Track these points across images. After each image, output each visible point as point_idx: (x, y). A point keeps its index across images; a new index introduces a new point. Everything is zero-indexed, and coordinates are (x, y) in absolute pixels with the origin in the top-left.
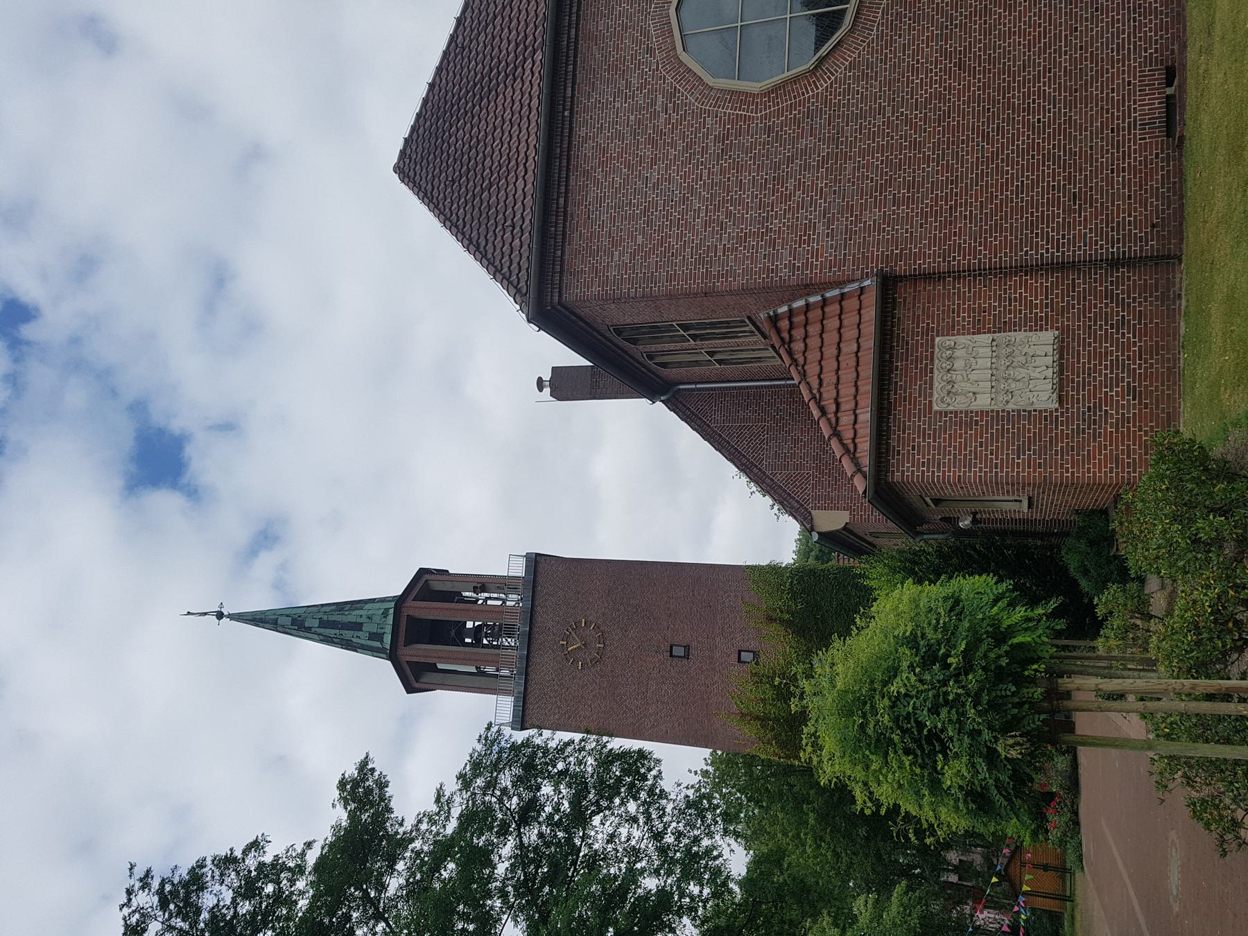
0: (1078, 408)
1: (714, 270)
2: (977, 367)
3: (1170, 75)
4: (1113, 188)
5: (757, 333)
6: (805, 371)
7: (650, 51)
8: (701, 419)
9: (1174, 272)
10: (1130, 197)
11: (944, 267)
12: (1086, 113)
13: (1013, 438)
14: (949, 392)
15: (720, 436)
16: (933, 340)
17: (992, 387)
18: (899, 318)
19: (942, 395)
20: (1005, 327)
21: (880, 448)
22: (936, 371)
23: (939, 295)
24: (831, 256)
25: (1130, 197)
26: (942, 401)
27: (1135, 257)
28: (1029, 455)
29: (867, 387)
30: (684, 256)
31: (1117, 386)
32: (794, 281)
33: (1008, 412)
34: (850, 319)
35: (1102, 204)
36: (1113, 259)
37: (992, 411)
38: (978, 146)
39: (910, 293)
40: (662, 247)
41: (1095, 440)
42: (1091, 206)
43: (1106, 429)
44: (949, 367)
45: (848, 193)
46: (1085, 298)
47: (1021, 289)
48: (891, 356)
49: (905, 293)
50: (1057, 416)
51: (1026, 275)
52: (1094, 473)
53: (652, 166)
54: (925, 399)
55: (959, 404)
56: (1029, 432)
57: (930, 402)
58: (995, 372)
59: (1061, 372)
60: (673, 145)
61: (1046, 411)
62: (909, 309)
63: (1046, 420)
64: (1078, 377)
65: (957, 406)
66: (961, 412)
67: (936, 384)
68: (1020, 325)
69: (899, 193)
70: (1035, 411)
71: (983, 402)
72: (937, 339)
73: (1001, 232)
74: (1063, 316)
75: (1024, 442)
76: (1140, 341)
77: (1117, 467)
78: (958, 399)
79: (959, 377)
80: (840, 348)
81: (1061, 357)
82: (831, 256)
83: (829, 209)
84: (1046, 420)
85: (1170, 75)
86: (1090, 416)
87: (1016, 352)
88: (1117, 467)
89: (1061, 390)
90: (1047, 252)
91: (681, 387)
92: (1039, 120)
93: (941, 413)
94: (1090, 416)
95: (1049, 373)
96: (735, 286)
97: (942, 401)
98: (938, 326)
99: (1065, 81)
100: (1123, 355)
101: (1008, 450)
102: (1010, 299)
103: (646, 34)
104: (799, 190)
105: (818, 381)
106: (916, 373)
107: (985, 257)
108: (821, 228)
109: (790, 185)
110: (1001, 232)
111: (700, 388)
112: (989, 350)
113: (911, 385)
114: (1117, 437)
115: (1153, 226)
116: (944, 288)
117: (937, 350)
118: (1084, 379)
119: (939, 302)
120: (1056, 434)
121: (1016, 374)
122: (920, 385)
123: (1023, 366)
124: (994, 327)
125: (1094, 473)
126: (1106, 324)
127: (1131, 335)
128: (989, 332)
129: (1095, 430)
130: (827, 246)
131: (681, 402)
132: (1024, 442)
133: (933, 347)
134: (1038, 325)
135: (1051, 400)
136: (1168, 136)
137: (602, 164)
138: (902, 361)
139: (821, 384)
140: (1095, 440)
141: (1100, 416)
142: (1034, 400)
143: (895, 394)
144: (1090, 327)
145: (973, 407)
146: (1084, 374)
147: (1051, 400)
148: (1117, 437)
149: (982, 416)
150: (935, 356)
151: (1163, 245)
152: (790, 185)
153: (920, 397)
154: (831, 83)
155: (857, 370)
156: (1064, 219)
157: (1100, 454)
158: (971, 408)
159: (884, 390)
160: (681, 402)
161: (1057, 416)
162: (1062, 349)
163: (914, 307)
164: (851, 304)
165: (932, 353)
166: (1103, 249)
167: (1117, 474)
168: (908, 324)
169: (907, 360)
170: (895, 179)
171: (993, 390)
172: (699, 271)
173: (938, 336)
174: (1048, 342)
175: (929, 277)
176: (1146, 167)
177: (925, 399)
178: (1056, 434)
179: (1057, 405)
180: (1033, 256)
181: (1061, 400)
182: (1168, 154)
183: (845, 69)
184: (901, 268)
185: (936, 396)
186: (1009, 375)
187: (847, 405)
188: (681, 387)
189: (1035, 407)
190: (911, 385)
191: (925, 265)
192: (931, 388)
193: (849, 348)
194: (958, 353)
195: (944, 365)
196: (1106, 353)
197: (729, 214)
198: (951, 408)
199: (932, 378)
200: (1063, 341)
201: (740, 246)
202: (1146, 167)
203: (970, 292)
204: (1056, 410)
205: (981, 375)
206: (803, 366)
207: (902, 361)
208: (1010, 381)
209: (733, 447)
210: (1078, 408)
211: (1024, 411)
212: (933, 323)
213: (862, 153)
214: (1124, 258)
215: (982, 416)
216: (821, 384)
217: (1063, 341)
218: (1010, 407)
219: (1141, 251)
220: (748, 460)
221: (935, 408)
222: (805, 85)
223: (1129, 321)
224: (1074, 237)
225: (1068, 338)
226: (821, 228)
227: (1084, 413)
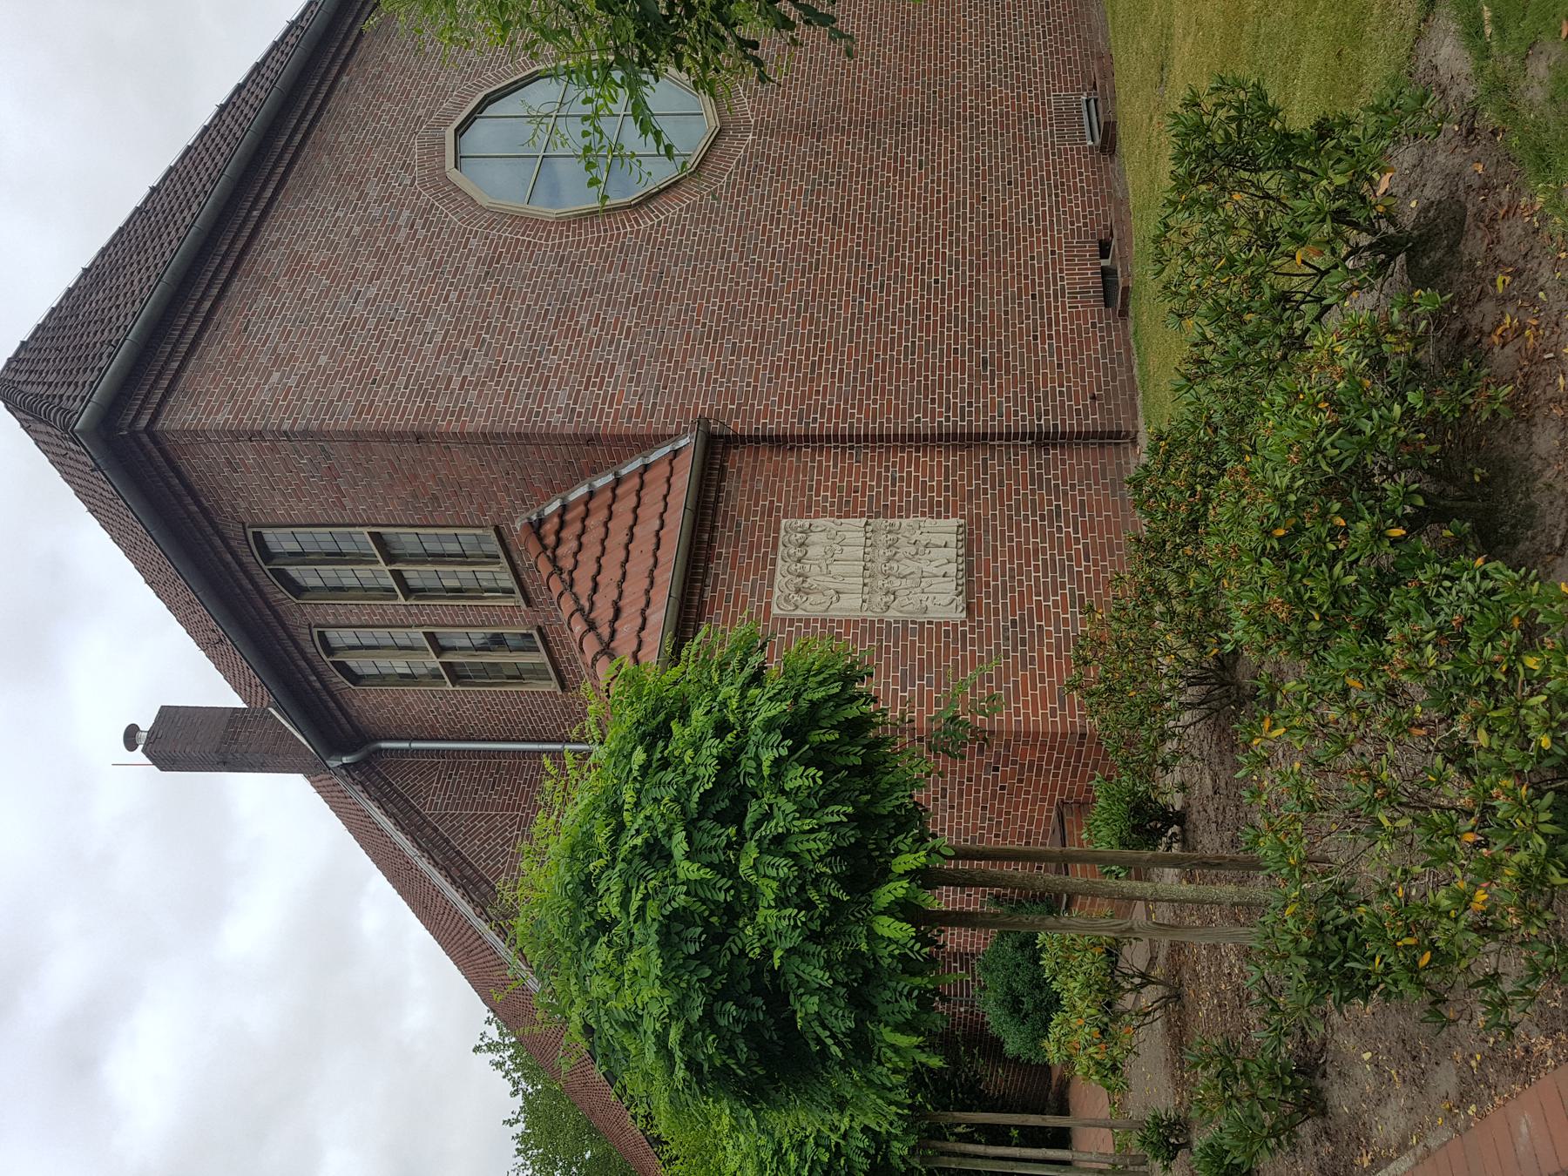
0: (997, 622)
1: (440, 405)
2: (842, 556)
3: (1104, 250)
4: (1036, 355)
5: (503, 560)
6: (572, 580)
7: (406, 167)
8: (407, 801)
9: (1126, 455)
10: (1060, 366)
11: (799, 429)
12: (999, 278)
13: (896, 660)
14: (798, 591)
15: (435, 830)
16: (778, 522)
17: (865, 585)
18: (728, 493)
19: (787, 592)
20: (888, 511)
21: (687, 613)
22: (779, 562)
23: (790, 469)
24: (632, 403)
25: (1060, 366)
26: (787, 600)
27: (1072, 432)
28: (921, 687)
29: (666, 576)
30: (393, 385)
31: (1055, 594)
32: (569, 429)
33: (889, 624)
34: (653, 495)
35: (1022, 372)
36: (1040, 433)
37: (864, 621)
38: (854, 300)
39: (748, 463)
40: (358, 371)
41: (1024, 667)
42: (1007, 373)
43: (1041, 652)
44: (800, 554)
45: (668, 337)
46: (1001, 482)
47: (910, 467)
48: (712, 539)
49: (739, 461)
50: (963, 633)
51: (918, 451)
52: (1026, 716)
53: (371, 279)
54: (760, 600)
55: (812, 607)
56: (921, 652)
57: (768, 605)
58: (869, 565)
59: (969, 571)
60: (412, 260)
61: (947, 624)
62: (745, 482)
63: (947, 637)
64: (996, 579)
65: (809, 608)
66: (816, 621)
67: (778, 577)
68: (908, 510)
69: (741, 342)
70: (930, 623)
71: (850, 605)
72: (784, 521)
73: (883, 394)
74: (970, 502)
75: (912, 666)
76: (1085, 537)
77: (1062, 708)
78: (812, 598)
79: (815, 569)
80: (632, 534)
81: (969, 553)
82: (632, 403)
83: (638, 351)
84: (947, 637)
85: (1104, 250)
86: (1015, 633)
87: (902, 540)
88: (1062, 708)
89: (970, 595)
90: (945, 421)
91: (384, 745)
92: (936, 281)
93: (783, 620)
94: (1015, 633)
95: (952, 568)
96: (470, 428)
97: (787, 600)
98: (786, 505)
99: (971, 245)
100: (1061, 554)
101: (887, 676)
102: (894, 479)
103: (407, 151)
104: (596, 326)
105: (590, 584)
106: (749, 564)
107: (858, 422)
108: (621, 370)
109: (583, 320)
110: (883, 394)
111: (418, 750)
112: (862, 534)
113: (739, 580)
114: (1059, 665)
115: (1093, 398)
116: (799, 459)
117: (782, 533)
118: (1004, 583)
119: (790, 476)
120: (964, 657)
121: (902, 567)
122: (754, 581)
123: (912, 558)
124: (870, 510)
125: (1026, 716)
126: (1034, 514)
127: (1071, 530)
128: (862, 515)
129: (1024, 653)
130: (629, 393)
131: (378, 774)
132: (912, 666)
133: (777, 531)
134: (935, 510)
135: (954, 605)
136: (1106, 306)
137: (291, 272)
138: (728, 547)
139: (595, 589)
140: (1024, 667)
141: (1032, 633)
142: (929, 603)
143: (714, 591)
144: (1010, 518)
145: (834, 613)
146: (1003, 575)
147: (954, 605)
148: (1059, 665)
149: (847, 627)
150: (780, 543)
151: (1110, 420)
152: (583, 320)
153: (752, 595)
154: (659, 223)
155: (655, 556)
156: (970, 385)
157: (1034, 688)
158: (832, 613)
159: (696, 581)
160: (378, 774)
161: (963, 633)
162: (970, 542)
163: (752, 479)
164: (656, 477)
165: (776, 539)
166: (1026, 421)
167: (1063, 718)
168: (742, 501)
169: (736, 546)
170: (737, 327)
171: (866, 589)
172: (413, 405)
173: (785, 517)
174: (949, 529)
175: (779, 442)
176: (1080, 336)
177: (760, 600)
178: (964, 657)
179: (964, 615)
180: (926, 425)
181: (969, 609)
182: (1108, 325)
183: (681, 210)
184: (738, 426)
185: (777, 592)
186: (891, 568)
187: (631, 611)
188: (384, 745)
189: (931, 615)
190: (739, 580)
191: (773, 426)
192: (771, 585)
193: (645, 531)
194: (813, 537)
195: (792, 551)
196: (1036, 551)
197: (480, 342)
198: (799, 612)
199: (773, 572)
200: (971, 533)
201: (491, 381)
202: (1080, 336)
203: (835, 466)
204: (963, 623)
205: (849, 572)
206: (571, 572)
207: (728, 547)
208: (891, 578)
209: (453, 848)
210: (997, 622)
211: (913, 622)
212: (779, 500)
213: (694, 296)
214: (1056, 433)
215: (847, 627)
216: (595, 589)
217: (971, 533)
218: (892, 614)
219: (1079, 425)
220: (475, 871)
221: (775, 610)
222: (622, 220)
223: (1066, 512)
224: (985, 406)
225: (978, 528)
226: (621, 370)
227: (1006, 629)
